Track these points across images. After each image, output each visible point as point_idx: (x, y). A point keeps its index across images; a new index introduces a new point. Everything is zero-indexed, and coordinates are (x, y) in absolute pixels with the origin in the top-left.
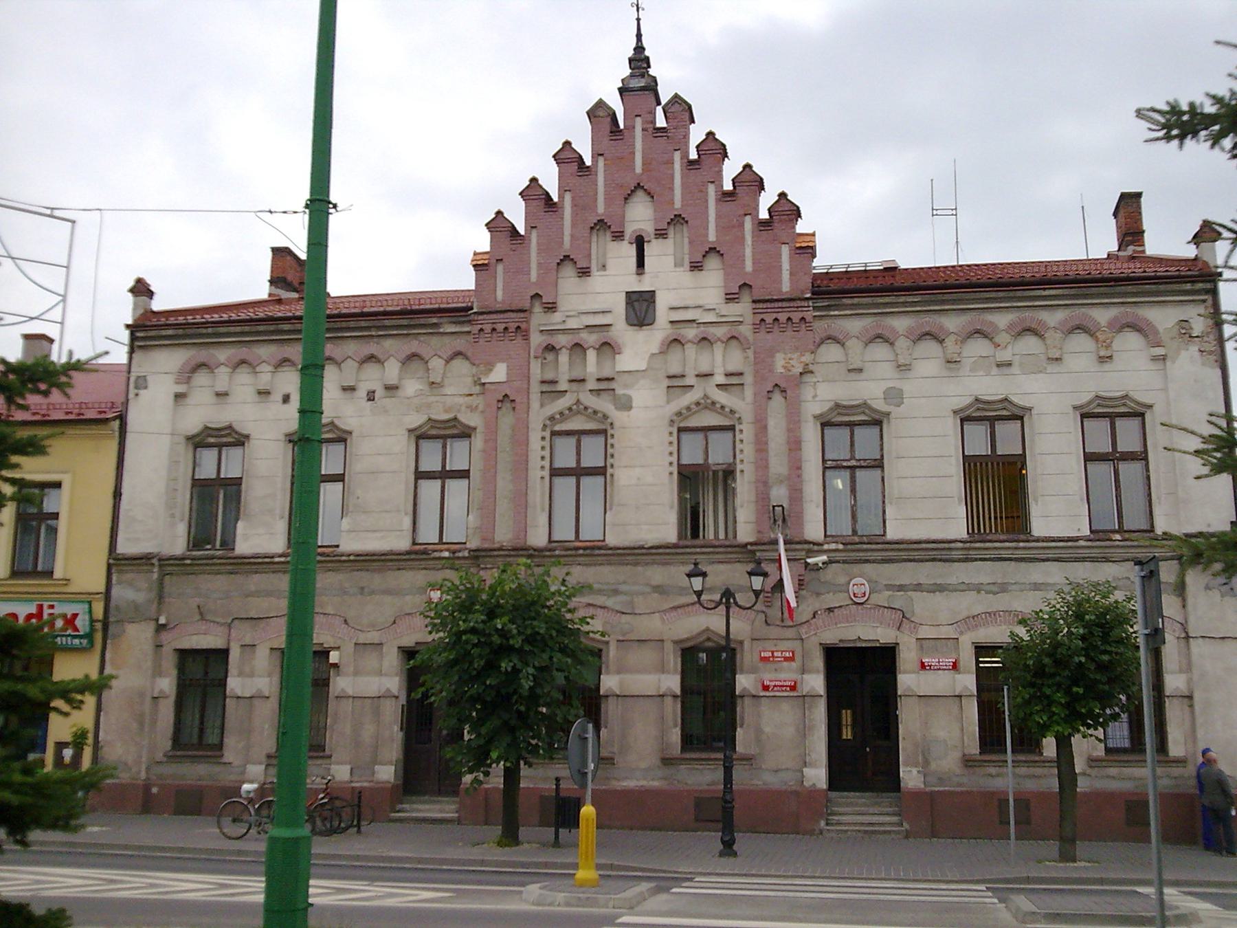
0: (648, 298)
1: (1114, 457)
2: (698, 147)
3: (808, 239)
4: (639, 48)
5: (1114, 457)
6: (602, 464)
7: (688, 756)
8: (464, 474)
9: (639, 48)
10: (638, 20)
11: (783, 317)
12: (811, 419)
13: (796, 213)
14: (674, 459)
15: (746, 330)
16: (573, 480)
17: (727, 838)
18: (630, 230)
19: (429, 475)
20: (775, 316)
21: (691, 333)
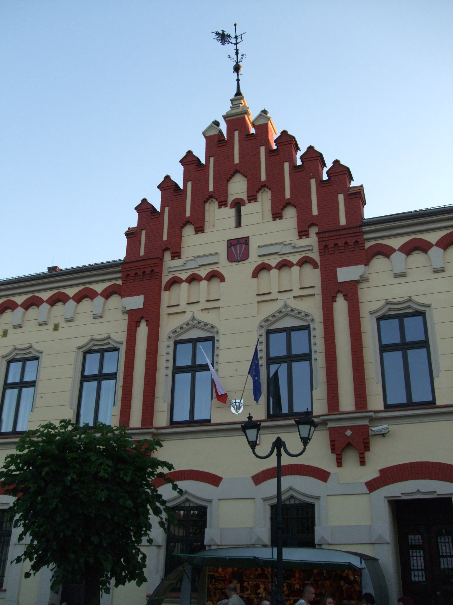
0: (245, 241)
1: (404, 346)
4: (238, 93)
5: (404, 346)
6: (307, 351)
8: (113, 376)
9: (238, 93)
10: (238, 80)
11: (341, 243)
12: (368, 315)
15: (315, 256)
18: (230, 199)
19: (13, 386)
21: (273, 261)
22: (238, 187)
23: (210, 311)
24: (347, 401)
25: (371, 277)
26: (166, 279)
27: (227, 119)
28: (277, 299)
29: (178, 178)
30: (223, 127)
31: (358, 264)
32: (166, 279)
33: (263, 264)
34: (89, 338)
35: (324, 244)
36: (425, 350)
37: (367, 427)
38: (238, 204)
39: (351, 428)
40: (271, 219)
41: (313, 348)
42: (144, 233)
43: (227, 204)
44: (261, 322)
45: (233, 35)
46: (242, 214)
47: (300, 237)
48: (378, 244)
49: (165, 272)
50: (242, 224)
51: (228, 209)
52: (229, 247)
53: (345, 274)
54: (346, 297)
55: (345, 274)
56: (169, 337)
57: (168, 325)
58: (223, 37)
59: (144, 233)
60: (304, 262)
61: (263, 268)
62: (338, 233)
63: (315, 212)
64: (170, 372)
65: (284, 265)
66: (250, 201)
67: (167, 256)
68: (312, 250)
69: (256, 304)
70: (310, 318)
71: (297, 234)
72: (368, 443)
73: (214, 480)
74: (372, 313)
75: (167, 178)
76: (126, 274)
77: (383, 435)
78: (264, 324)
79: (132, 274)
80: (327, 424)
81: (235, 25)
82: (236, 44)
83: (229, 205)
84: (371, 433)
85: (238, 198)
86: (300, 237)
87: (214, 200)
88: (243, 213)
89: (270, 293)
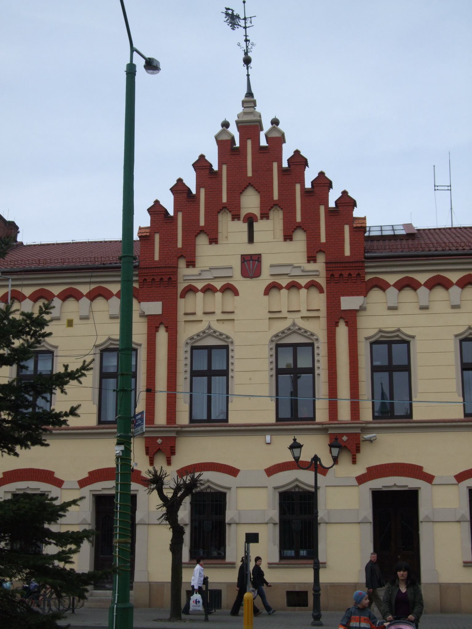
0: (257, 259)
2: (288, 160)
3: (361, 221)
4: (250, 94)
7: (282, 562)
9: (250, 94)
10: (248, 75)
11: (345, 273)
12: (363, 340)
13: (353, 204)
14: (274, 366)
15: (322, 281)
16: (205, 379)
17: (315, 614)
18: (244, 213)
20: (144, 277)
21: (284, 282)
22: (251, 202)
23: (225, 322)
24: (344, 413)
25: (369, 307)
26: (181, 287)
27: (239, 125)
28: (286, 318)
29: (191, 183)
30: (234, 130)
31: (358, 295)
32: (181, 287)
33: (274, 282)
34: (106, 337)
35: (331, 273)
36: (407, 373)
37: (358, 435)
38: (250, 220)
39: (347, 434)
40: (282, 238)
41: (317, 365)
42: (157, 237)
43: (239, 218)
44: (272, 338)
45: (242, 17)
46: (255, 229)
47: (309, 261)
48: (376, 277)
49: (180, 279)
50: (255, 240)
51: (241, 222)
52: (242, 262)
53: (348, 303)
54: (347, 324)
55: (348, 303)
56: (187, 343)
57: (187, 332)
58: (233, 19)
59: (157, 237)
60: (312, 285)
61: (273, 287)
62: (344, 265)
63: (323, 239)
64: (188, 375)
65: (293, 286)
66: (262, 218)
67: (182, 263)
68: (318, 275)
69: (268, 320)
70: (315, 337)
71: (306, 259)
72: (359, 447)
73: (233, 472)
74: (367, 339)
75: (180, 181)
76: (143, 279)
77: (371, 441)
78: (274, 339)
79: (149, 279)
80: (328, 431)
81: (244, 2)
82: (245, 28)
83: (242, 218)
84: (361, 439)
85: (251, 213)
86: (309, 261)
87: (227, 211)
88: (255, 229)
89: (280, 312)
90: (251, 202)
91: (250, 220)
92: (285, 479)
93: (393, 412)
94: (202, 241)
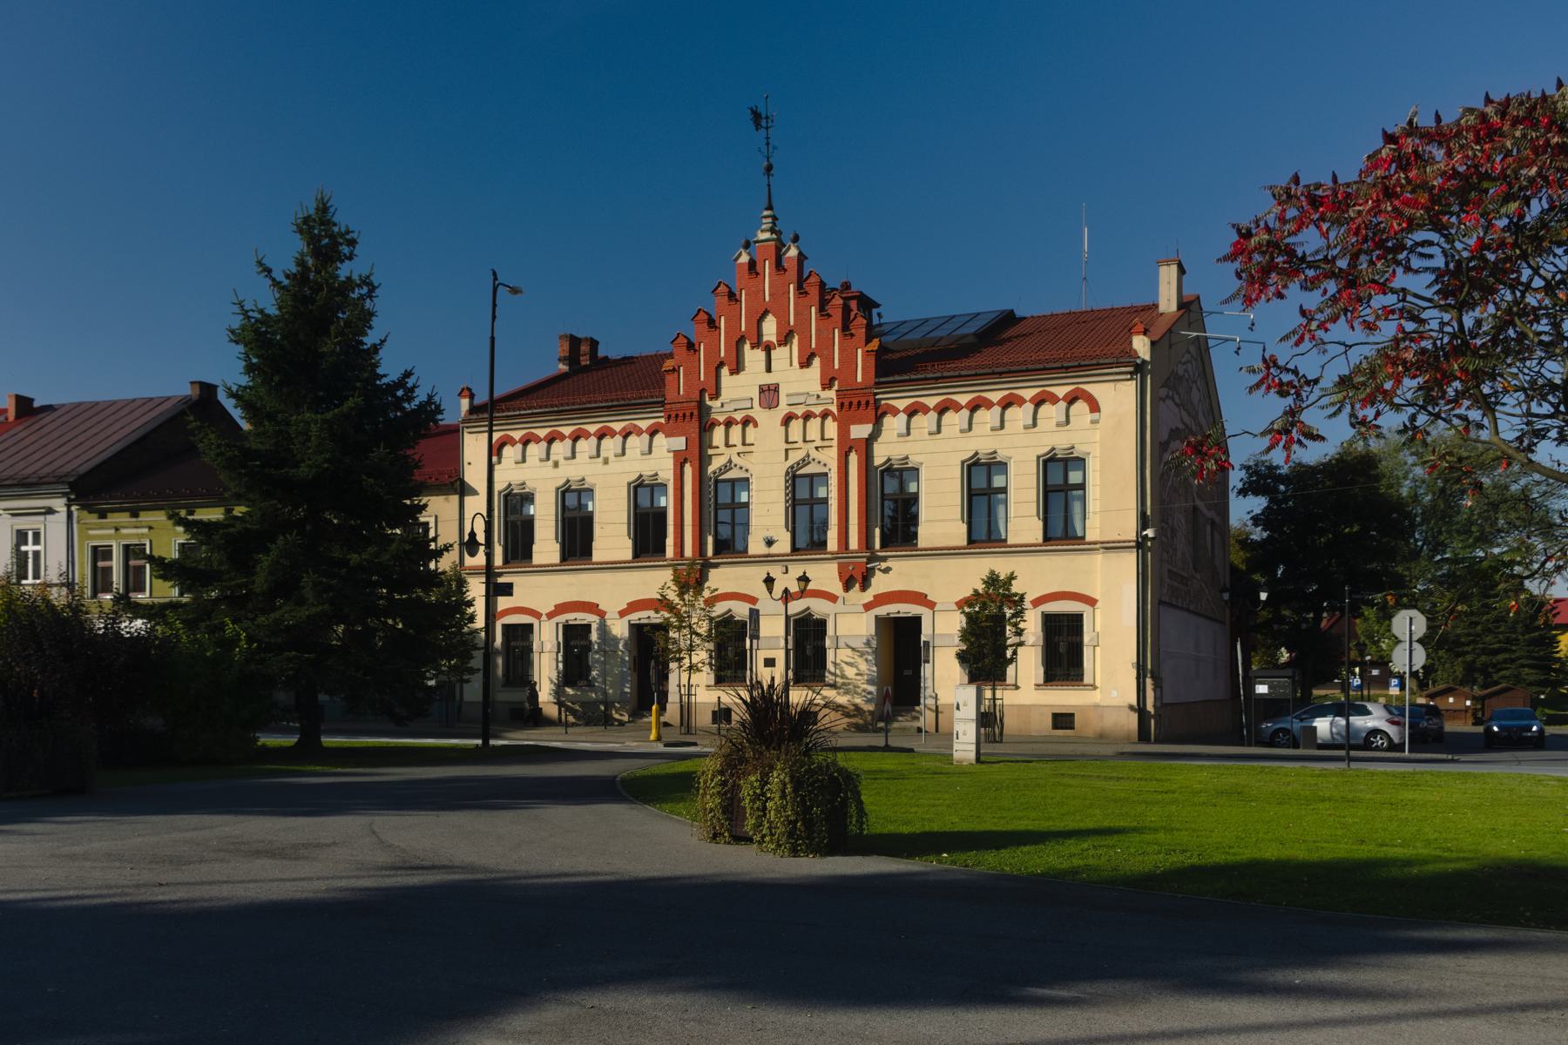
38: (768, 349)
53: (860, 431)
58: (757, 117)
90: (770, 328)
91: (768, 349)
92: (796, 607)
93: (730, 547)
94: (725, 371)
